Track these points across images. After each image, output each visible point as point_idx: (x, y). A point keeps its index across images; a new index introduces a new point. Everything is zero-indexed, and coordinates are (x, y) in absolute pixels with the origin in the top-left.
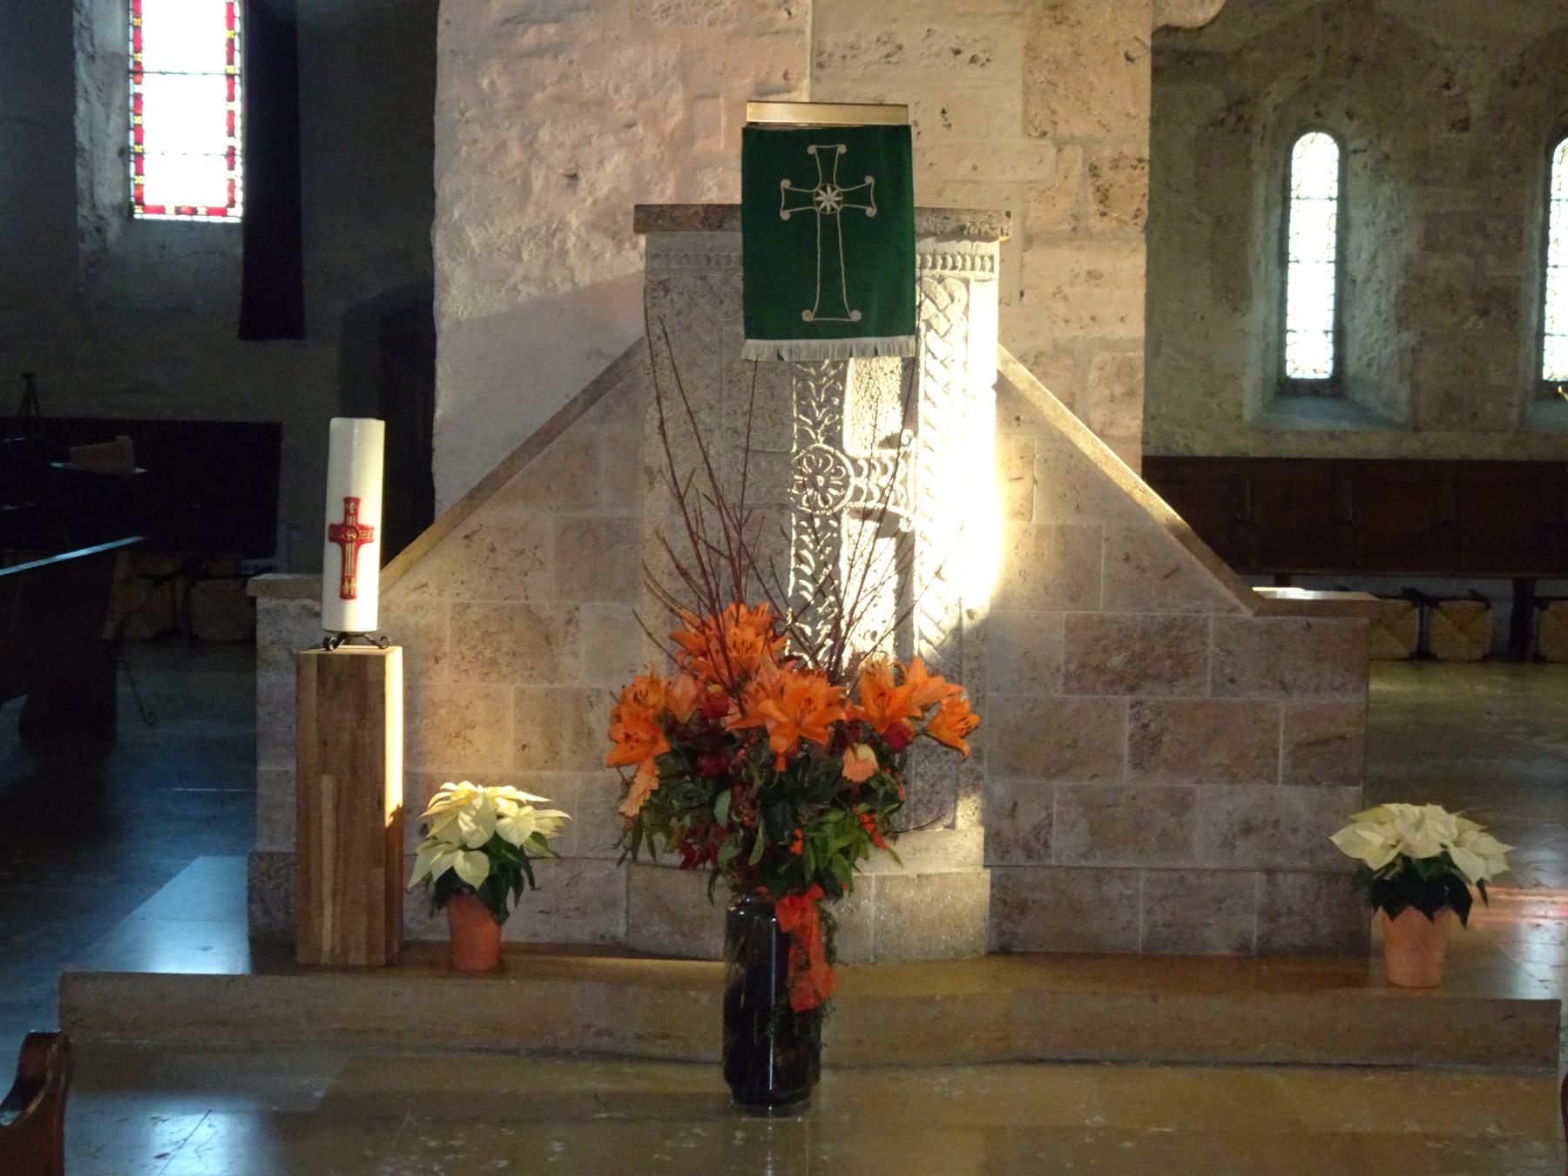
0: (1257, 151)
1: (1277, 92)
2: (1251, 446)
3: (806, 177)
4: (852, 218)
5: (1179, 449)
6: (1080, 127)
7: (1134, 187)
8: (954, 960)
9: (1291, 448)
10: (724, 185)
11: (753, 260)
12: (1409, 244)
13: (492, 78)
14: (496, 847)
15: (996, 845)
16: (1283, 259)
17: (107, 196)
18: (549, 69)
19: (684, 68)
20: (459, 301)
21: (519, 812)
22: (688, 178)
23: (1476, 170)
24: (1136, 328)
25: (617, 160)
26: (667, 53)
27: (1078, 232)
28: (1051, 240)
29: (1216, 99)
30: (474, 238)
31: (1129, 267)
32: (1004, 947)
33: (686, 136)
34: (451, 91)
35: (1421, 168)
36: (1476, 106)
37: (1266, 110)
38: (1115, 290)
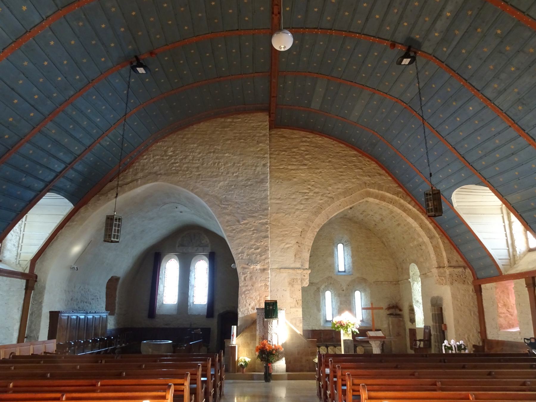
0: (321, 294)
1: (323, 287)
2: (322, 329)
3: (269, 306)
4: (273, 309)
5: (314, 329)
6: (295, 297)
7: (300, 302)
8: (283, 372)
9: (327, 329)
10: (263, 306)
11: (265, 312)
12: (339, 304)
13: (243, 296)
14: (245, 362)
15: (287, 363)
16: (325, 306)
17: (191, 301)
18: (248, 295)
19: (259, 295)
20: (240, 315)
21: (248, 360)
22: (259, 305)
23: (345, 296)
24: (301, 316)
25: (254, 303)
26: (258, 293)
27: (295, 307)
28: (293, 308)
29: (316, 288)
30: (241, 310)
31: (300, 310)
32: (287, 370)
33: (259, 301)
34: (240, 297)
35: (339, 295)
36: (344, 288)
37: (321, 289)
38: (299, 312)
